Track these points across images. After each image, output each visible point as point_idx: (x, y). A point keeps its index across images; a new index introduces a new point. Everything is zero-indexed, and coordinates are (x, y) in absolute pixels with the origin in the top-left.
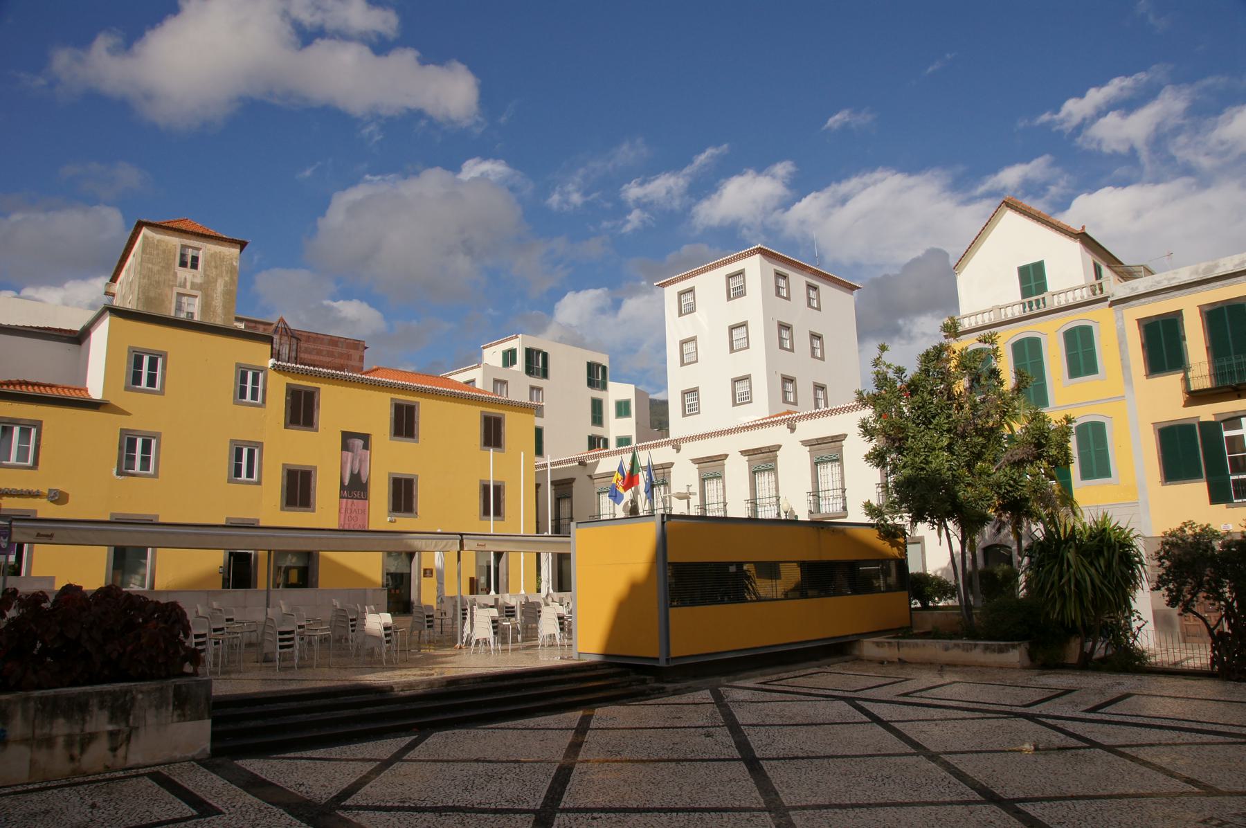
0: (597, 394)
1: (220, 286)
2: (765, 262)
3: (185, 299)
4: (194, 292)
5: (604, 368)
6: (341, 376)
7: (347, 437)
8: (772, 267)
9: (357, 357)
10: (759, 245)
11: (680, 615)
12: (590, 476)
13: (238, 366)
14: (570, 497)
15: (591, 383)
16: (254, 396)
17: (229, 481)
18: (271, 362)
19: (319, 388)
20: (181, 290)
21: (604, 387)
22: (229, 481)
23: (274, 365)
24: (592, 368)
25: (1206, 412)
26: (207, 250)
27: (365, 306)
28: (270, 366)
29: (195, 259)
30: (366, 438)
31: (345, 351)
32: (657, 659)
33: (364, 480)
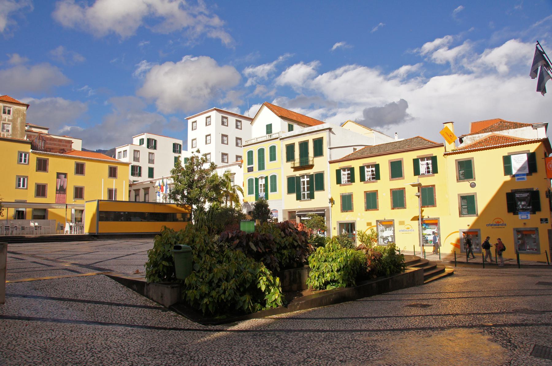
0: (177, 155)
1: (19, 120)
2: (218, 113)
3: (5, 125)
4: (9, 123)
5: (180, 145)
6: (56, 155)
7: (59, 175)
8: (220, 115)
9: (69, 146)
10: (215, 108)
11: (101, 223)
12: (153, 187)
13: (19, 152)
14: (148, 194)
15: (174, 151)
16: (25, 161)
17: (16, 188)
18: (31, 150)
19: (48, 159)
20: (4, 122)
21: (180, 152)
22: (16, 188)
23: (32, 152)
24: (175, 145)
25: (298, 173)
26: (13, 108)
27: (205, 62)
28: (30, 152)
29: (9, 111)
30: (66, 175)
31: (64, 144)
32: (95, 233)
33: (65, 188)
